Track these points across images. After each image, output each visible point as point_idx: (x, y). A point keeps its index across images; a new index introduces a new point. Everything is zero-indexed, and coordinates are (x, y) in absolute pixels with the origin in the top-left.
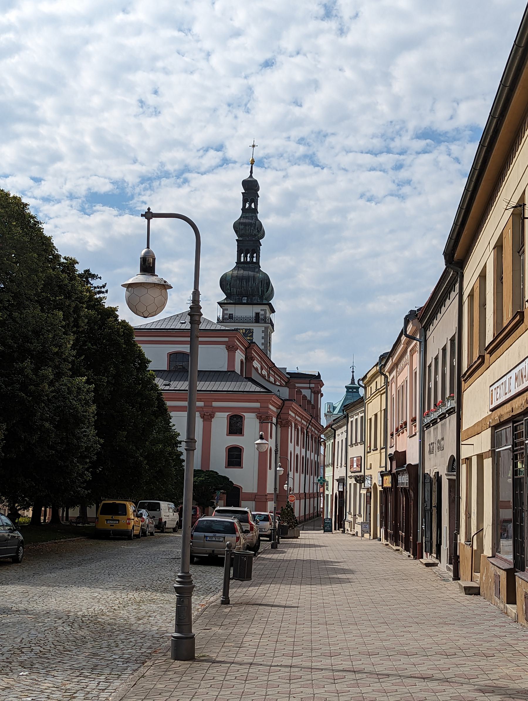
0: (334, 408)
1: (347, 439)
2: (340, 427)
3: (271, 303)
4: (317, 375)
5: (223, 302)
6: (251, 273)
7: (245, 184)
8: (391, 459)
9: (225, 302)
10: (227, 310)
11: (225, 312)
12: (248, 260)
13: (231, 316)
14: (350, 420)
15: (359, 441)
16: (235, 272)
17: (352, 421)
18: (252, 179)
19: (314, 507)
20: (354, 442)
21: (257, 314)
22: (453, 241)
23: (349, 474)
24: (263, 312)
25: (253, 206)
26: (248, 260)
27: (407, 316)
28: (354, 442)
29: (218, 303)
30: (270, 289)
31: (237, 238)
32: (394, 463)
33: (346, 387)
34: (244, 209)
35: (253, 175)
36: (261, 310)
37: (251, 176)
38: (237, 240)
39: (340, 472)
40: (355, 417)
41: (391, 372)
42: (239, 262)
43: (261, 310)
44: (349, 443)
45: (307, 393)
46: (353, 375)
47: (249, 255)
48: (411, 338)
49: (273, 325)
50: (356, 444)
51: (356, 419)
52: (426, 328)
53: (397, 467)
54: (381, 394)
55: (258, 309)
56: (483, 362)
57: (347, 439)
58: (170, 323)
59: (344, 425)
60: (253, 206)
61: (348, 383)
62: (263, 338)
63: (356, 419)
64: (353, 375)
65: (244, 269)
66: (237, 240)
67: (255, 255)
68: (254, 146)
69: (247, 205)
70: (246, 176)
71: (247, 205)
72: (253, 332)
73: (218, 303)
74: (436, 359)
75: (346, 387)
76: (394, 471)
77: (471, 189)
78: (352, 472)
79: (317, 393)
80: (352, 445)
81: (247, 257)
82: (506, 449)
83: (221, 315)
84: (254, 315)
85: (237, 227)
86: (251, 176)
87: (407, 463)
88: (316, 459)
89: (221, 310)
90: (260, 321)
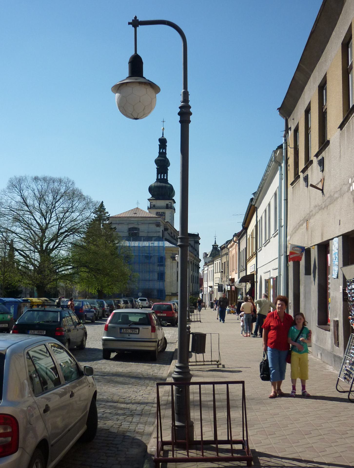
0: (207, 255)
1: (213, 270)
2: (211, 265)
3: (174, 199)
4: (197, 234)
5: (150, 199)
6: (164, 184)
7: (160, 140)
8: (230, 280)
9: (151, 199)
10: (152, 203)
11: (151, 204)
12: (162, 177)
13: (154, 206)
14: (215, 262)
15: (218, 271)
16: (156, 184)
17: (215, 263)
18: (163, 138)
19: (215, 298)
20: (216, 272)
21: (167, 205)
22: (248, 210)
23: (215, 284)
24: (170, 204)
25: (164, 151)
26: (162, 177)
27: (234, 235)
28: (216, 272)
29: (148, 199)
30: (173, 192)
31: (157, 167)
32: (231, 282)
33: (212, 245)
34: (160, 153)
35: (164, 136)
36: (169, 203)
37: (163, 136)
38: (156, 168)
39: (211, 284)
40: (217, 262)
41: (230, 248)
42: (157, 179)
43: (169, 203)
44: (214, 272)
45: (192, 243)
46: (215, 241)
47: (162, 175)
48: (235, 242)
49: (174, 209)
50: (217, 272)
51: (217, 263)
52: (239, 240)
53: (232, 283)
54: (227, 255)
55: (167, 202)
56: (253, 257)
57: (213, 270)
58: (129, 213)
59: (212, 264)
60: (164, 151)
61: (213, 243)
62: (170, 216)
63: (217, 263)
64: (215, 241)
65: (161, 182)
66: (156, 168)
67: (165, 175)
68: (163, 122)
69: (161, 151)
70: (160, 136)
71: (161, 151)
72: (165, 214)
73: (148, 199)
74: (242, 251)
75: (212, 245)
76: (231, 285)
77: (249, 209)
78: (216, 284)
79: (197, 243)
80: (215, 273)
81: (161, 176)
82: (50, 394)
83: (149, 205)
84: (166, 205)
85: (157, 162)
86: (163, 136)
87: (310, 160)
88: (197, 275)
89: (149, 202)
90: (169, 208)
